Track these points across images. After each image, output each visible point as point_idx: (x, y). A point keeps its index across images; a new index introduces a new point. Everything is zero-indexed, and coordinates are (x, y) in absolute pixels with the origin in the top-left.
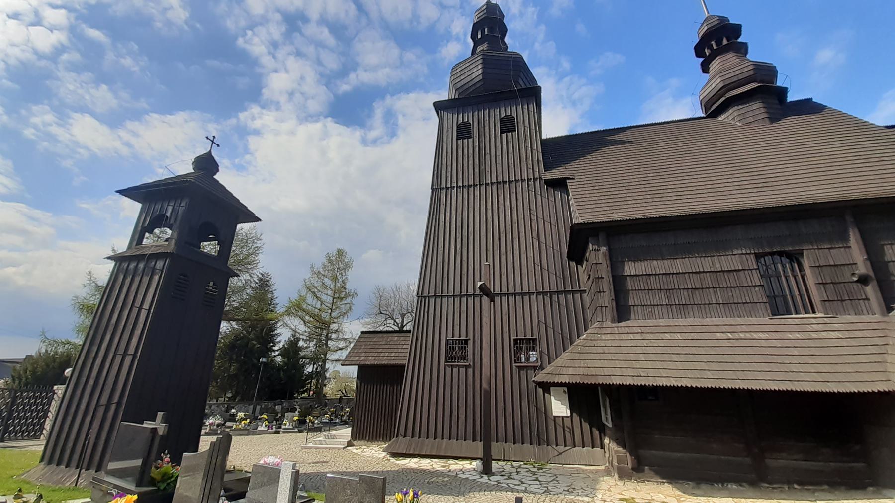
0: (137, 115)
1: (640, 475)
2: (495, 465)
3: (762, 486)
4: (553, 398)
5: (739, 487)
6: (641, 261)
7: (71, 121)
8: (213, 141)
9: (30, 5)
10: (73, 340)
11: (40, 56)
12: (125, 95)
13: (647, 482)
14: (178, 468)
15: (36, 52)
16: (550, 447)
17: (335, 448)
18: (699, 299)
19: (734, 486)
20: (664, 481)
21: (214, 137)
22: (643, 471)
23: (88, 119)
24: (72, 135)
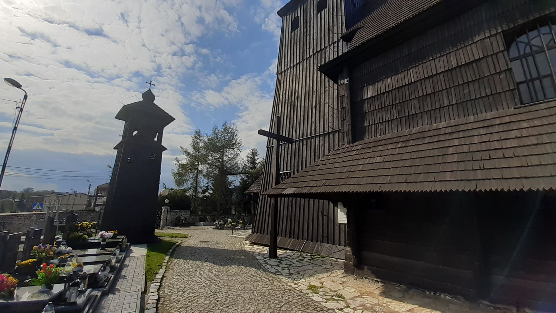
0: (226, 84)
1: (360, 272)
2: (280, 252)
3: (482, 304)
4: (339, 210)
5: (454, 299)
6: (377, 82)
7: (205, 95)
8: (151, 84)
9: (178, 47)
10: (174, 188)
11: (188, 69)
12: (221, 76)
13: (365, 279)
14: (102, 241)
15: (186, 67)
16: (334, 245)
17: (242, 238)
18: (429, 104)
19: (448, 297)
20: (379, 280)
21: (151, 81)
22: (362, 269)
23: (211, 92)
24: (207, 101)
